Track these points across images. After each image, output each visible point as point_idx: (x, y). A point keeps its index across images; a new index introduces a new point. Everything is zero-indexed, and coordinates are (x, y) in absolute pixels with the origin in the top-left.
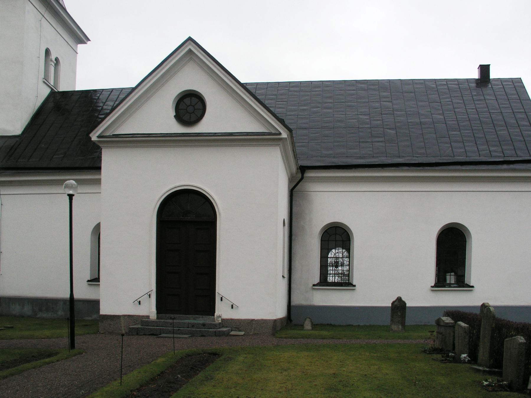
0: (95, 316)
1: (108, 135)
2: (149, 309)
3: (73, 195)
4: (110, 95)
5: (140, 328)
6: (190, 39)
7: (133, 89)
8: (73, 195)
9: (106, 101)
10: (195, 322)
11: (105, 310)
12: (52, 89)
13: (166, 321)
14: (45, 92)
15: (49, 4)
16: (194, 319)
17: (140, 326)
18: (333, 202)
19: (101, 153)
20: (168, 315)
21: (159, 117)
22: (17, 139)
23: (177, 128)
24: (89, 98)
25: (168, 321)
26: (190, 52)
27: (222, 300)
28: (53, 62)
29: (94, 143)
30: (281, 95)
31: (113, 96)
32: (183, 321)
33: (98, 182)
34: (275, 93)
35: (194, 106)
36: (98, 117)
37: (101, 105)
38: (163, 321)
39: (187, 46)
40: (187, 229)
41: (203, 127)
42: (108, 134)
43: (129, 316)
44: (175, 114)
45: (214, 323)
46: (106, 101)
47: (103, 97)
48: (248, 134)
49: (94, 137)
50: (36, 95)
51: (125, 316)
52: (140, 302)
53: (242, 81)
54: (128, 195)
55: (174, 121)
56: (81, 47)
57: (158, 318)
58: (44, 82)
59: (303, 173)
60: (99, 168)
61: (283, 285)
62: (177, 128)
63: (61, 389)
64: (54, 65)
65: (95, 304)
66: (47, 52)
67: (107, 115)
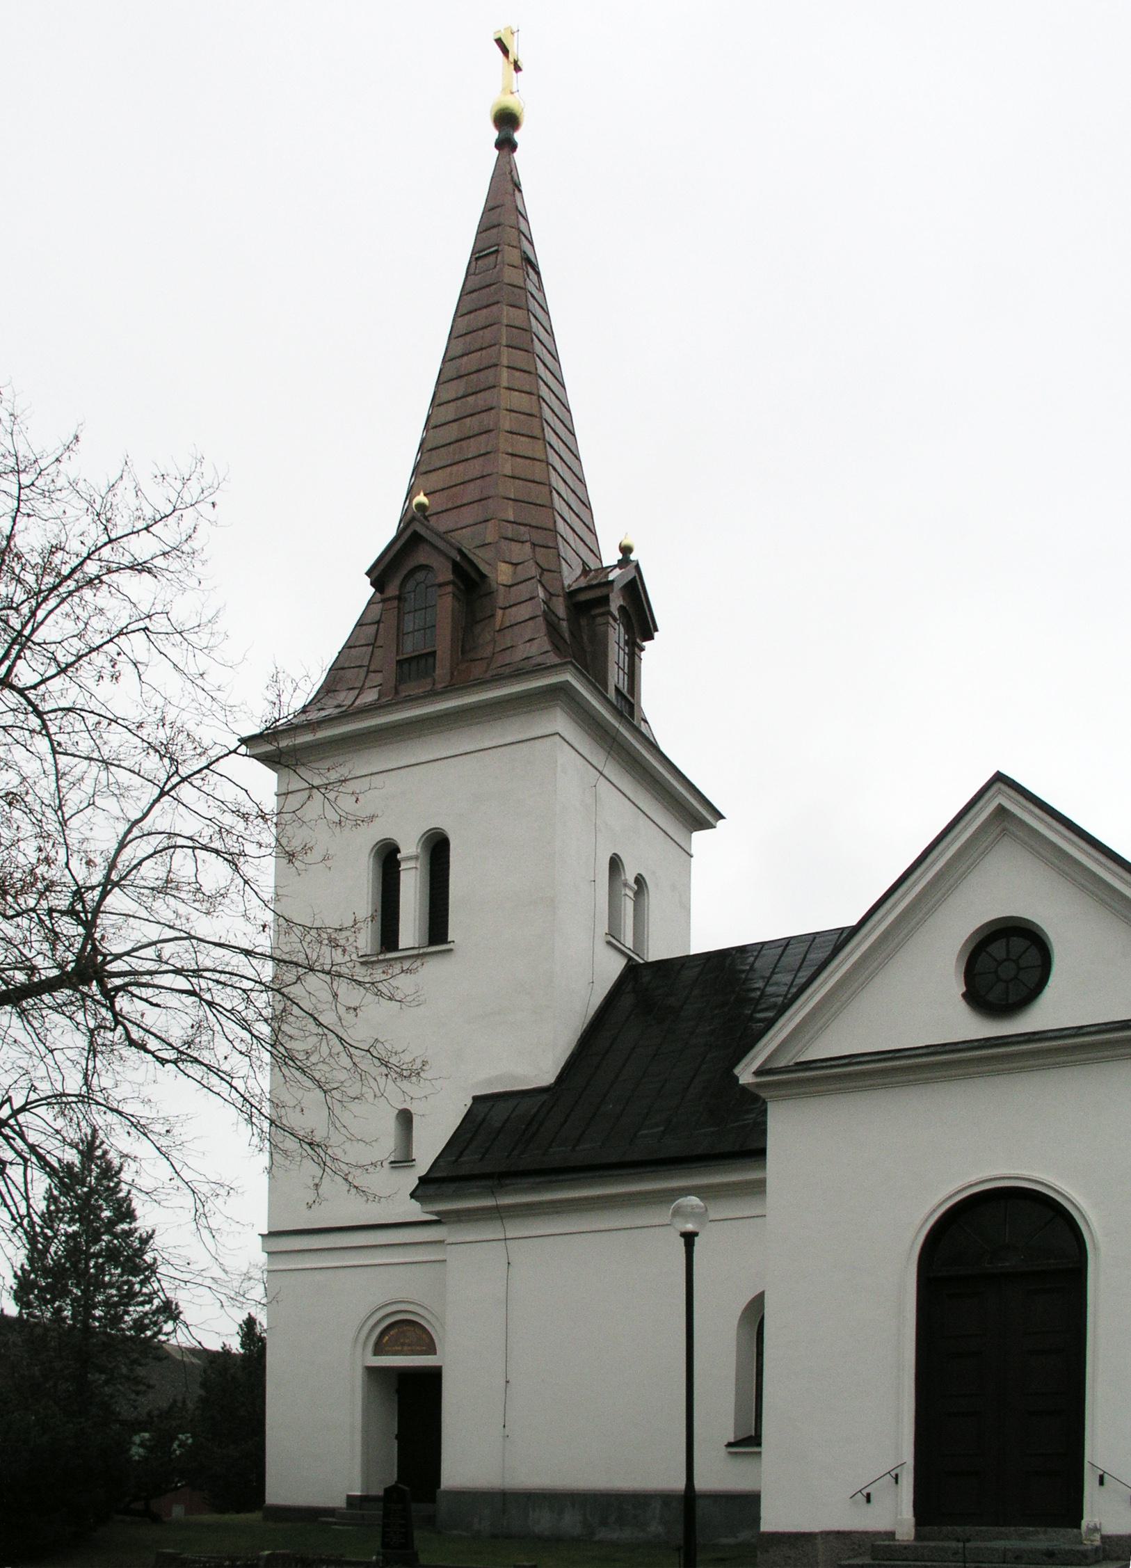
0: (744, 1536)
1: (782, 1065)
2: (895, 1513)
3: (695, 1234)
4: (781, 956)
5: (869, 1565)
6: (999, 778)
7: (853, 931)
8: (695, 1234)
9: (773, 973)
10: (1023, 1545)
11: (773, 1519)
12: (630, 959)
13: (941, 1544)
14: (614, 966)
15: (614, 739)
16: (1022, 1537)
17: (867, 1560)
19: (764, 1112)
20: (947, 1529)
21: (924, 1001)
22: (545, 1097)
23: (972, 1027)
24: (728, 971)
25: (946, 1544)
26: (1004, 814)
27: (1101, 1482)
28: (631, 888)
29: (744, 1088)
31: (792, 959)
32: (989, 1544)
33: (758, 1188)
35: (1016, 962)
36: (751, 1018)
37: (760, 984)
38: (932, 1544)
39: (989, 801)
41: (1048, 1013)
42: (782, 1063)
43: (839, 1534)
44: (964, 989)
45: (1081, 1548)
46: (773, 973)
47: (764, 965)
49: (745, 1074)
50: (592, 974)
51: (828, 1533)
52: (868, 1496)
55: (962, 1007)
56: (699, 838)
57: (918, 1536)
58: (609, 943)
60: (761, 1153)
62: (972, 1027)
64: (631, 894)
65: (748, 1503)
66: (615, 864)
67: (782, 1009)
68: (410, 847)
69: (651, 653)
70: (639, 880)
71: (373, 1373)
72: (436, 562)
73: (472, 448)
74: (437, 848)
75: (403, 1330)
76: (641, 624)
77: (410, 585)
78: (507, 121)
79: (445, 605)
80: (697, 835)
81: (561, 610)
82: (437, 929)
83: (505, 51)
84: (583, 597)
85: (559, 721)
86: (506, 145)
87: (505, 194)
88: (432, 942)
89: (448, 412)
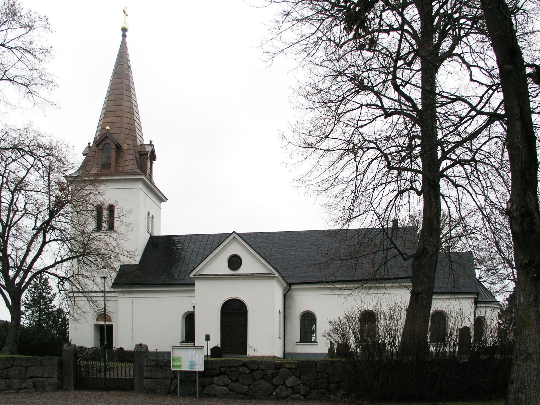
6: (234, 232)
14: (148, 236)
18: (307, 300)
30: (282, 240)
34: (278, 239)
40: (234, 314)
41: (241, 271)
48: (261, 274)
49: (191, 275)
54: (207, 301)
59: (290, 286)
61: (281, 342)
62: (229, 271)
66: (148, 213)
69: (155, 163)
72: (112, 143)
73: (117, 114)
76: (153, 157)
77: (105, 147)
78: (124, 30)
79: (114, 153)
80: (163, 203)
81: (138, 156)
83: (125, 13)
84: (142, 153)
85: (140, 185)
86: (124, 36)
87: (123, 47)
89: (111, 103)
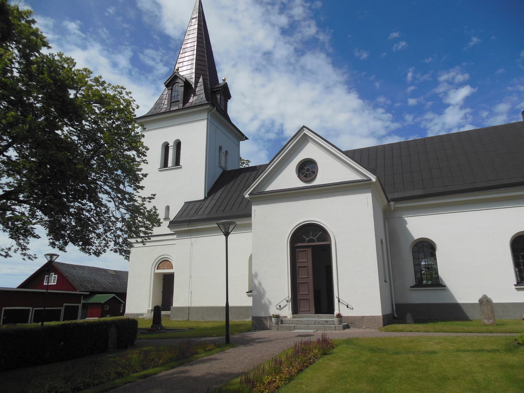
12: (224, 170)
21: (288, 178)
22: (200, 203)
23: (302, 184)
40: (311, 250)
41: (318, 182)
53: (343, 150)
55: (296, 176)
62: (302, 184)
63: (278, 377)
66: (220, 148)
68: (171, 144)
70: (226, 152)
71: (156, 275)
74: (178, 144)
75: (164, 262)
82: (177, 162)
88: (176, 166)
